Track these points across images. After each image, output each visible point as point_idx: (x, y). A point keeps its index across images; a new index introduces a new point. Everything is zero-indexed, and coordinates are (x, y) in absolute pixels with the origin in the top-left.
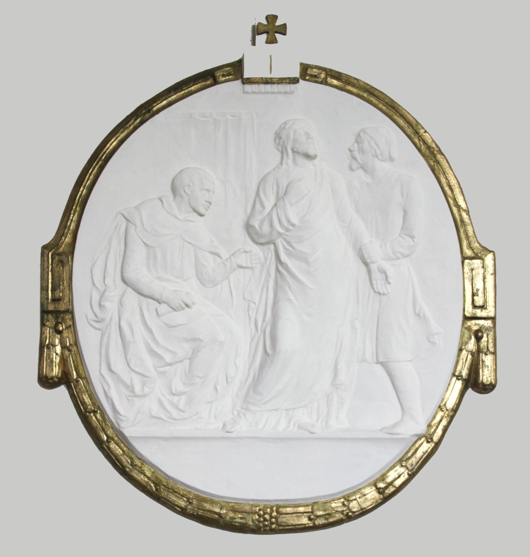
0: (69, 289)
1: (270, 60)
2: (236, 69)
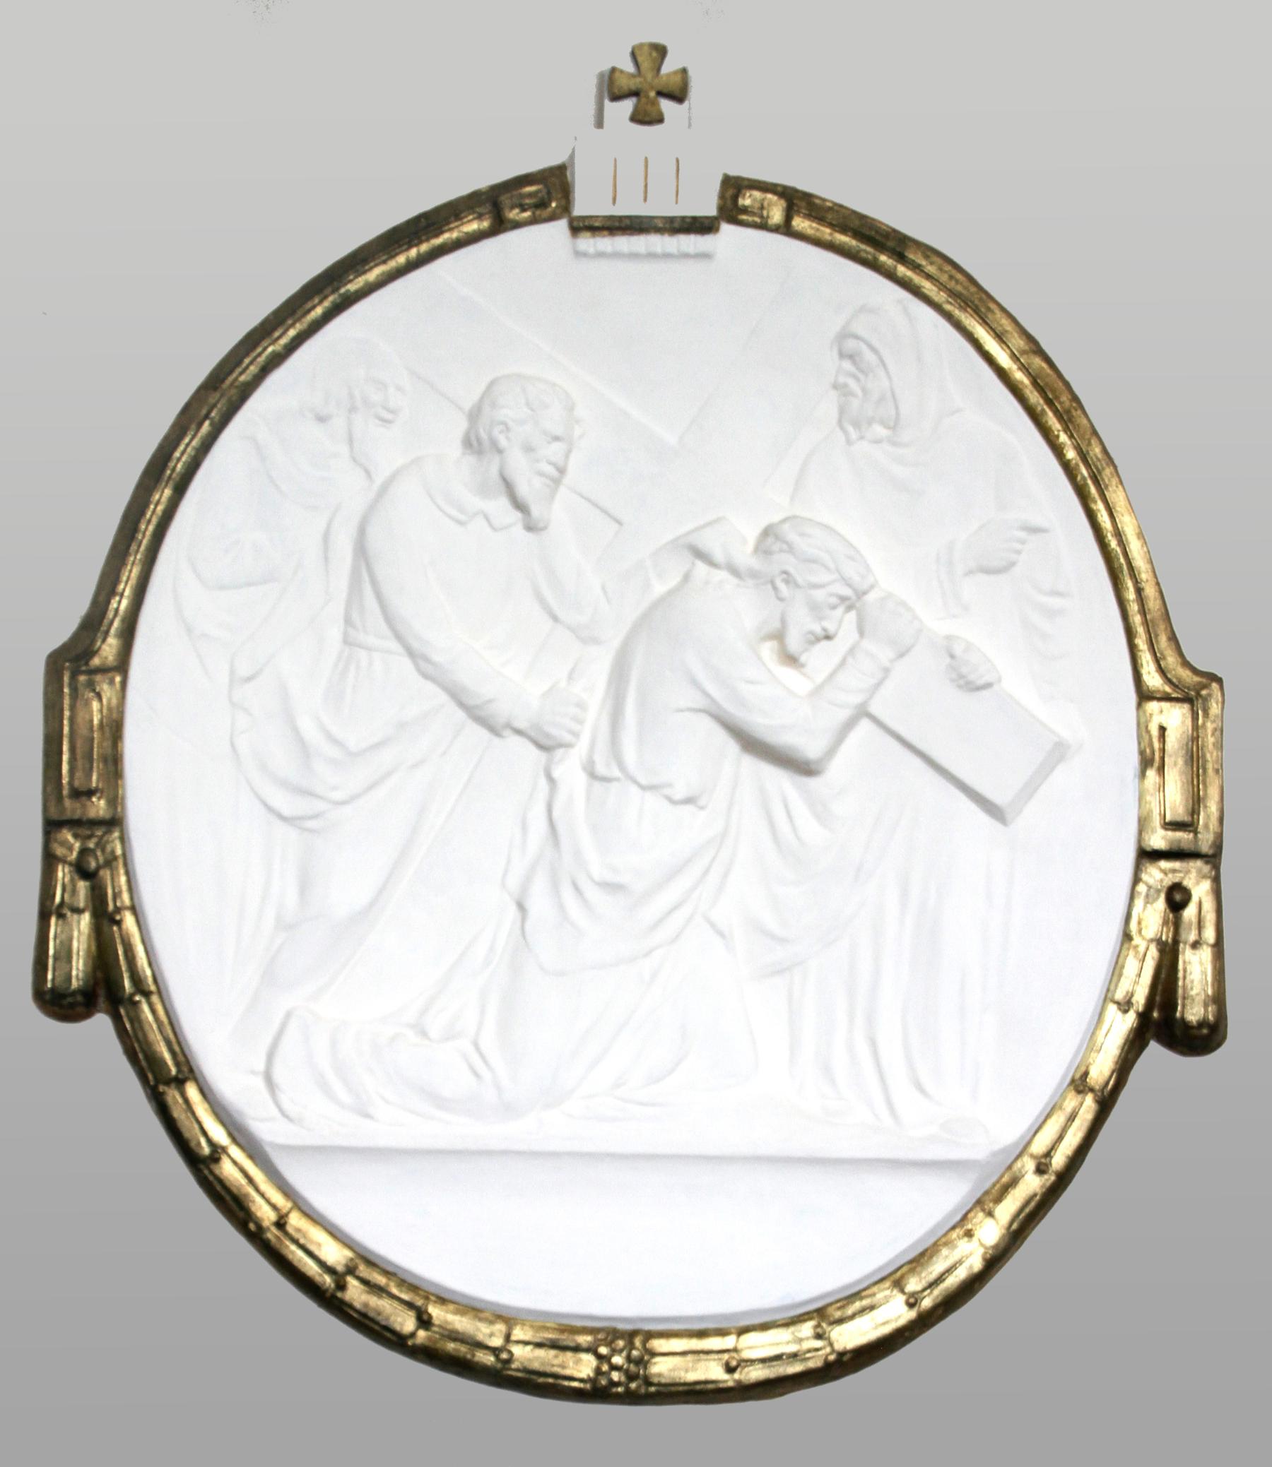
0: (168, 457)
1: (643, 168)
2: (541, 195)
